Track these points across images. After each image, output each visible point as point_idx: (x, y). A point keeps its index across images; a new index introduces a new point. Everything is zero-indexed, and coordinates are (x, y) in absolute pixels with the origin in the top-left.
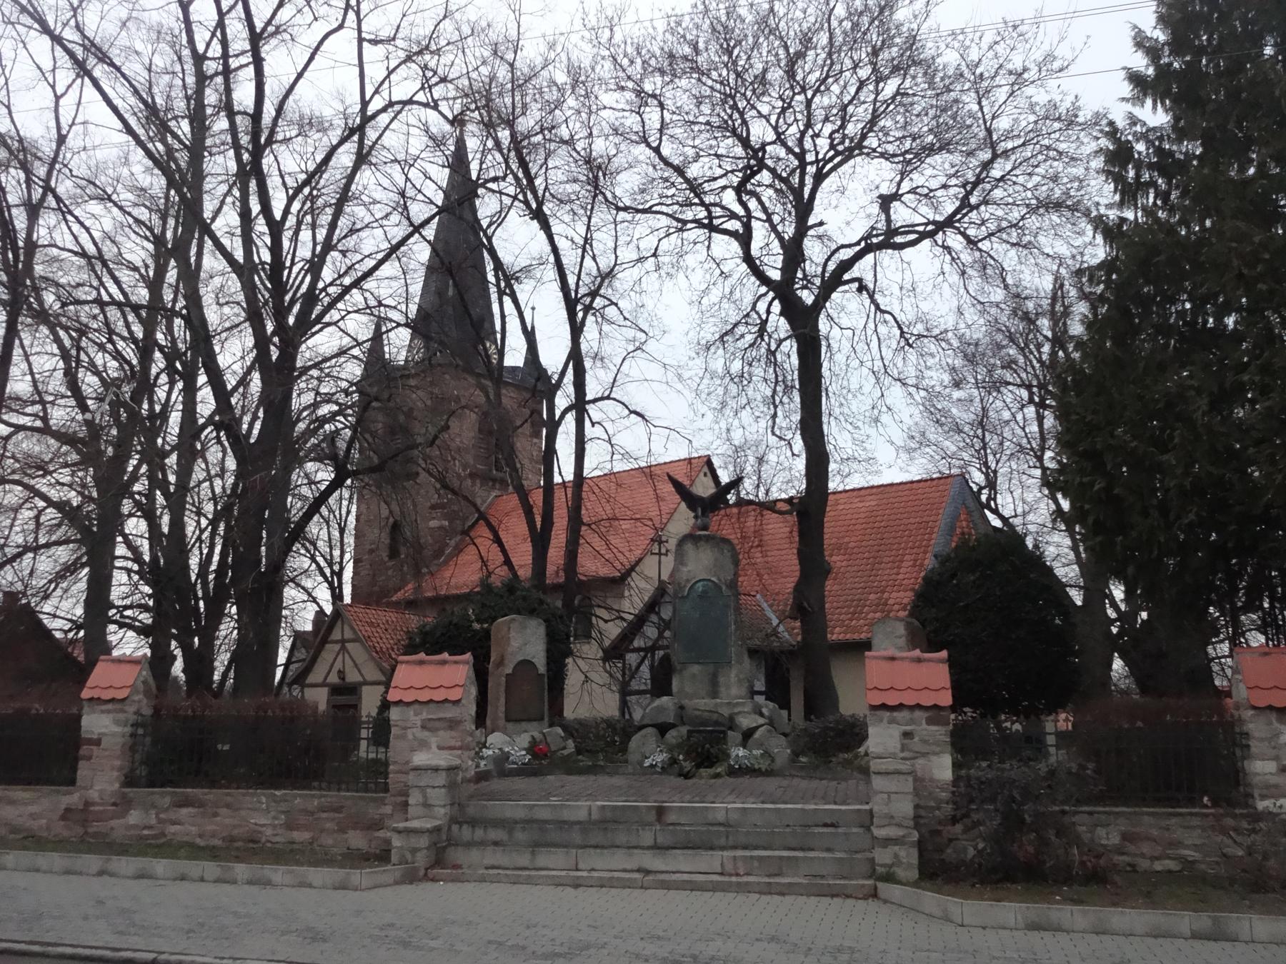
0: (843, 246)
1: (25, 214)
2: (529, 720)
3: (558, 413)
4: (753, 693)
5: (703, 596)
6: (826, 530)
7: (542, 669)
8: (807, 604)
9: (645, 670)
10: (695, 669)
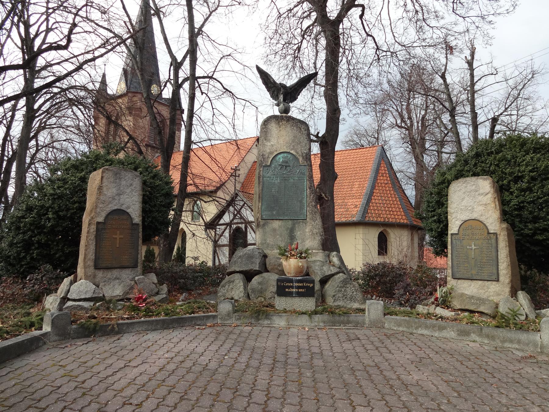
1: (9, 71)
3: (180, 81)
5: (285, 165)
6: (319, 171)
7: (137, 218)
9: (227, 234)
10: (276, 224)
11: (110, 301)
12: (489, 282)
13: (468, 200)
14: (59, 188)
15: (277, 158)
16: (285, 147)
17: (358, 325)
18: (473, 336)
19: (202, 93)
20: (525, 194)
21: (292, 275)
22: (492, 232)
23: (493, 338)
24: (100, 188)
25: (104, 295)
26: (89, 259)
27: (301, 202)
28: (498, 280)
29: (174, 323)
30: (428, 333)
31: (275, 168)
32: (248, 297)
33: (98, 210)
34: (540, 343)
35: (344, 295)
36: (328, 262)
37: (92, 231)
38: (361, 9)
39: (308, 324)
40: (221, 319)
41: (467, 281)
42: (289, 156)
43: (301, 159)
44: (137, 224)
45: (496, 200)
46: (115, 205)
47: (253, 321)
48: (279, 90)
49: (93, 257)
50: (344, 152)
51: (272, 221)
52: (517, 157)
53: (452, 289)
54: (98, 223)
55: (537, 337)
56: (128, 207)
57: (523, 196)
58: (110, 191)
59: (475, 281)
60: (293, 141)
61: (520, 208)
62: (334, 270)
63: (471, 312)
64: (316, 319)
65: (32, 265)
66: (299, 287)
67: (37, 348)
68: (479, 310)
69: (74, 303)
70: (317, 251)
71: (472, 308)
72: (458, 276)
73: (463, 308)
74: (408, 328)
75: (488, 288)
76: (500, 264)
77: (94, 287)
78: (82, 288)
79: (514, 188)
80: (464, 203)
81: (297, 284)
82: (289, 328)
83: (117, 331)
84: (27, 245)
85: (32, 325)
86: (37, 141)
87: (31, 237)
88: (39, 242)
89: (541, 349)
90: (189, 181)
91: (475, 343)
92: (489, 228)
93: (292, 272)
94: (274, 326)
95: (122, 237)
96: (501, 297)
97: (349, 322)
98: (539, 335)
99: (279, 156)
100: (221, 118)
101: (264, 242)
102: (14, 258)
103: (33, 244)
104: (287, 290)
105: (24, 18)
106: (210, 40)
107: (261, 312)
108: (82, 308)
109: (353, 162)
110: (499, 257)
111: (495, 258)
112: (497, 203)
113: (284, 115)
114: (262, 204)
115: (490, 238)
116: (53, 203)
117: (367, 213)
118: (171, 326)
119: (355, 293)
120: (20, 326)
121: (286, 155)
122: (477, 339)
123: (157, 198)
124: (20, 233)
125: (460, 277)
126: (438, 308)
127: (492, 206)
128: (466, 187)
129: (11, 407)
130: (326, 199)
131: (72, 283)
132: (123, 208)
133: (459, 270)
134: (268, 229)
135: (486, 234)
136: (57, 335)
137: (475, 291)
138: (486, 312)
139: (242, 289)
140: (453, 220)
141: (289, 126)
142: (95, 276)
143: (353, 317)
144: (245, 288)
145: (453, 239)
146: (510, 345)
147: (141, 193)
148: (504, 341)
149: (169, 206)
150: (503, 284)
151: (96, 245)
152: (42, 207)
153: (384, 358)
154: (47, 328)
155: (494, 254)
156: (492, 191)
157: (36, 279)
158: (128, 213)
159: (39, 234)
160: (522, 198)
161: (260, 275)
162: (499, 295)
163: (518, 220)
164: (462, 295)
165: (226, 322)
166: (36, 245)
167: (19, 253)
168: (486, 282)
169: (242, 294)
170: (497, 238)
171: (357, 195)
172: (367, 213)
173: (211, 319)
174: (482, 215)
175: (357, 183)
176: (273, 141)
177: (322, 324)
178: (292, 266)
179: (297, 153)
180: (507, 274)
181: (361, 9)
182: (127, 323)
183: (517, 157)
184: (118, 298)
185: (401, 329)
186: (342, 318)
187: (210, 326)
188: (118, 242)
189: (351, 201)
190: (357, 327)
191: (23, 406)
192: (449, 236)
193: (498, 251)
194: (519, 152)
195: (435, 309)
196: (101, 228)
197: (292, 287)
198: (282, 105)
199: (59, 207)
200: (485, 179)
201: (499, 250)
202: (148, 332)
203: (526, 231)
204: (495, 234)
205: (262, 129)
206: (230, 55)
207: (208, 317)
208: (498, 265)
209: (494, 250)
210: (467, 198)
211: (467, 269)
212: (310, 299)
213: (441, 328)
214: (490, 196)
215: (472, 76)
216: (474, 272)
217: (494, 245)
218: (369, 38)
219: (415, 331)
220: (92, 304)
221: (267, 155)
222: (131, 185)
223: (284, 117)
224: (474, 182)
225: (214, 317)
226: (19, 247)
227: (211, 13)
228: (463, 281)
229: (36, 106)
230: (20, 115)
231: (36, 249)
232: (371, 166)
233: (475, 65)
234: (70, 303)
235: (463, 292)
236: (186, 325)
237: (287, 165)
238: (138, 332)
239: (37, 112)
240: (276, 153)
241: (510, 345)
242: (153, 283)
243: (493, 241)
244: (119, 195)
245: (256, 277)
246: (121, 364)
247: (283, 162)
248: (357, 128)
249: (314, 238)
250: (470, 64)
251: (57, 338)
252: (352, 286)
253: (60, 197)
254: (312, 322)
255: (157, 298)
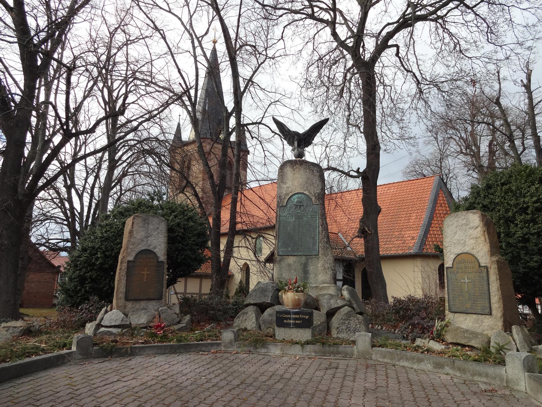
0: (389, 24)
2: (149, 299)
4: (335, 280)
5: (299, 205)
8: (368, 229)
10: (291, 260)
11: (135, 328)
12: (483, 316)
13: (460, 234)
14: (106, 232)
15: (292, 199)
16: (299, 189)
17: (347, 356)
18: (447, 369)
19: (252, 138)
20: (529, 225)
21: (290, 307)
22: (483, 265)
23: (463, 371)
24: (131, 232)
25: (130, 323)
26: (121, 292)
27: (314, 238)
28: (490, 314)
29: (182, 348)
30: (409, 366)
31: (290, 208)
32: (260, 327)
33: (129, 250)
34: (505, 377)
35: (348, 328)
36: (340, 295)
37: (123, 268)
38: (395, 48)
39: (301, 353)
40: (224, 346)
41: (463, 315)
42: (303, 196)
43: (313, 199)
44: (163, 262)
45: (486, 233)
46: (144, 246)
47: (252, 349)
48: (294, 137)
49: (124, 290)
50: (401, 184)
51: (287, 257)
52: (522, 188)
53: (448, 322)
54: (129, 262)
55: (501, 370)
56: (155, 248)
57: (527, 228)
58: (139, 234)
59: (470, 315)
60: (306, 183)
61: (525, 240)
62: (340, 303)
63: (463, 346)
64: (308, 349)
65: (86, 297)
66: (296, 319)
67: (62, 364)
68: (470, 344)
69: (106, 329)
70: (329, 285)
71: (463, 342)
72: (454, 309)
73: (454, 341)
74: (392, 360)
75: (482, 322)
76: (492, 298)
77: (123, 315)
78: (113, 317)
79: (519, 218)
80: (457, 237)
81: (294, 316)
82: (283, 357)
83: (132, 353)
84: (82, 280)
85: (65, 345)
86: (121, 186)
87: (85, 273)
88: (91, 277)
89: (506, 383)
90: (239, 220)
91: (447, 375)
92: (480, 261)
93: (290, 304)
94: (270, 354)
95: (149, 273)
96: (494, 331)
97: (338, 353)
98: (504, 369)
99: (294, 197)
100: (272, 159)
101: (280, 276)
102: (73, 291)
103: (86, 280)
104: (285, 321)
105: (108, 84)
106: (261, 89)
107: (258, 341)
108: (111, 334)
109: (410, 193)
110: (491, 291)
111: (486, 292)
112: (487, 236)
113: (298, 159)
114: (278, 241)
115: (482, 272)
116: (102, 244)
117: (425, 245)
118: (178, 351)
119: (358, 326)
120: (56, 346)
121: (300, 195)
122: (451, 372)
123: (189, 238)
124: (77, 270)
125: (456, 310)
126: (431, 341)
127: (482, 239)
128: (458, 221)
129: (16, 403)
130: (369, 232)
131: (106, 312)
132: (151, 248)
133: (454, 303)
134: (283, 264)
135: (477, 267)
136: (81, 354)
137: (470, 324)
138: (476, 346)
139: (254, 320)
140: (448, 254)
141: (302, 169)
142: (125, 307)
143: (342, 348)
144: (257, 319)
145: (448, 272)
146: (479, 379)
147: (166, 235)
148: (473, 375)
149: (203, 245)
150: (496, 318)
151: (127, 280)
152: (93, 248)
153: (440, 398)
154: (74, 348)
155: (486, 287)
156: (481, 225)
157: (86, 309)
158: (154, 253)
159: (91, 270)
160: (525, 230)
161: (272, 307)
162: (492, 329)
163: (523, 252)
164: (458, 328)
165: (229, 350)
166: (89, 280)
167: (76, 287)
168: (480, 316)
169: (254, 325)
170: (488, 272)
171: (414, 226)
172: (425, 245)
173: (215, 347)
174: (473, 249)
175: (414, 215)
176: (289, 184)
177: (313, 354)
178: (290, 299)
179: (311, 193)
180: (499, 307)
181: (395, 48)
182: (140, 347)
183: (522, 188)
184: (143, 326)
185: (386, 360)
186: (332, 349)
187: (214, 353)
188: (145, 277)
189: (408, 232)
190: (346, 357)
191: (25, 403)
192: (445, 270)
193: (489, 284)
194: (524, 183)
195: (429, 342)
196: (131, 265)
197: (290, 319)
198: (296, 150)
199: (106, 248)
200: (475, 213)
201: (490, 283)
202: (156, 355)
203: (532, 264)
204: (486, 267)
205: (279, 173)
206: (278, 101)
207: (212, 345)
208: (490, 299)
209: (485, 283)
210: (459, 232)
211: (462, 303)
212: (307, 330)
213: (420, 361)
214: (479, 229)
215: (530, 98)
216: (468, 305)
217: (485, 278)
218: (409, 74)
219: (397, 363)
220: (120, 330)
221: (283, 197)
222: (158, 228)
223: (299, 162)
224: (465, 216)
225: (219, 345)
226: (76, 282)
227: (259, 65)
228: (459, 314)
229: (116, 158)
230: (105, 165)
231: (89, 283)
232: (429, 197)
233: (533, 88)
234: (102, 329)
235: (460, 325)
236: (192, 350)
237: (301, 204)
238: (149, 355)
239: (118, 163)
240: (291, 194)
241: (479, 379)
242: (175, 313)
243: (485, 274)
244: (147, 237)
245: (268, 310)
246: (117, 378)
247: (297, 202)
248: (418, 158)
249: (326, 272)
250: (527, 87)
251: (81, 357)
252: (355, 319)
253: (107, 239)
254: (303, 352)
255: (176, 327)
